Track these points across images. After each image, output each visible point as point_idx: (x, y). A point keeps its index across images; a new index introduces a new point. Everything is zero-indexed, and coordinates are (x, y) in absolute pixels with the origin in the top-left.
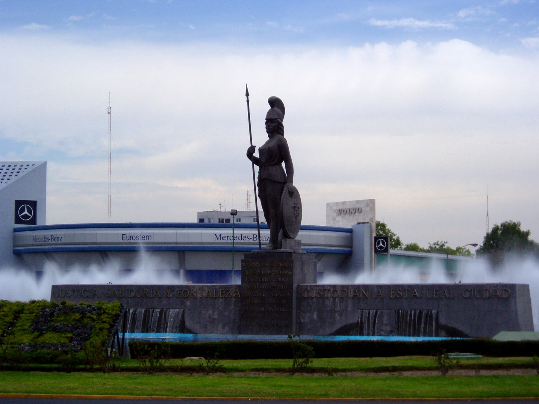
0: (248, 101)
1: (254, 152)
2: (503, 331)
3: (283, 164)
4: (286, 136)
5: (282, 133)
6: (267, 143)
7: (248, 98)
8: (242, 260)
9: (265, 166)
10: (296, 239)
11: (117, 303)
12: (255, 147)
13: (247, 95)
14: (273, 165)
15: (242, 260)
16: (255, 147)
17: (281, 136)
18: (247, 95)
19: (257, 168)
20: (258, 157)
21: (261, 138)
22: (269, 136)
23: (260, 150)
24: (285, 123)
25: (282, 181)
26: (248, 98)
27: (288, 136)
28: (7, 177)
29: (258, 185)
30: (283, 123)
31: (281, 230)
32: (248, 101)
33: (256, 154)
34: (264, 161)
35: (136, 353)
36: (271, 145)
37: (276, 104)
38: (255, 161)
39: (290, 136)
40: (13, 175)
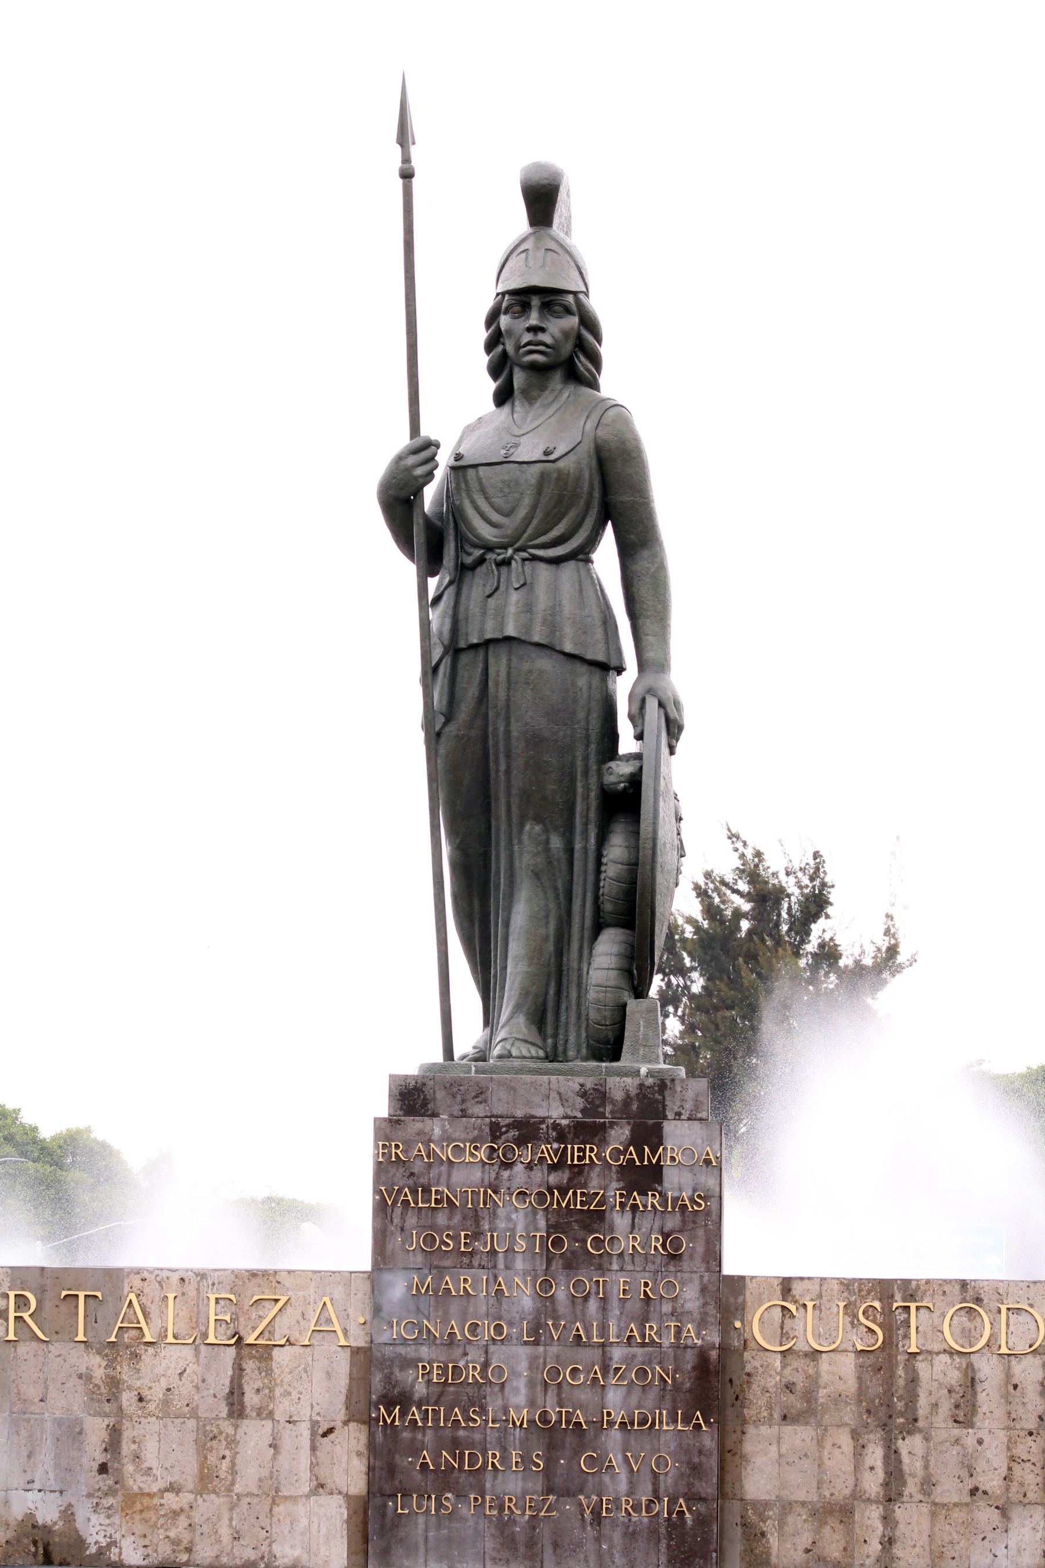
0: (407, 175)
3: (606, 558)
9: (506, 563)
14: (557, 561)
21: (462, 405)
22: (503, 397)
26: (406, 159)
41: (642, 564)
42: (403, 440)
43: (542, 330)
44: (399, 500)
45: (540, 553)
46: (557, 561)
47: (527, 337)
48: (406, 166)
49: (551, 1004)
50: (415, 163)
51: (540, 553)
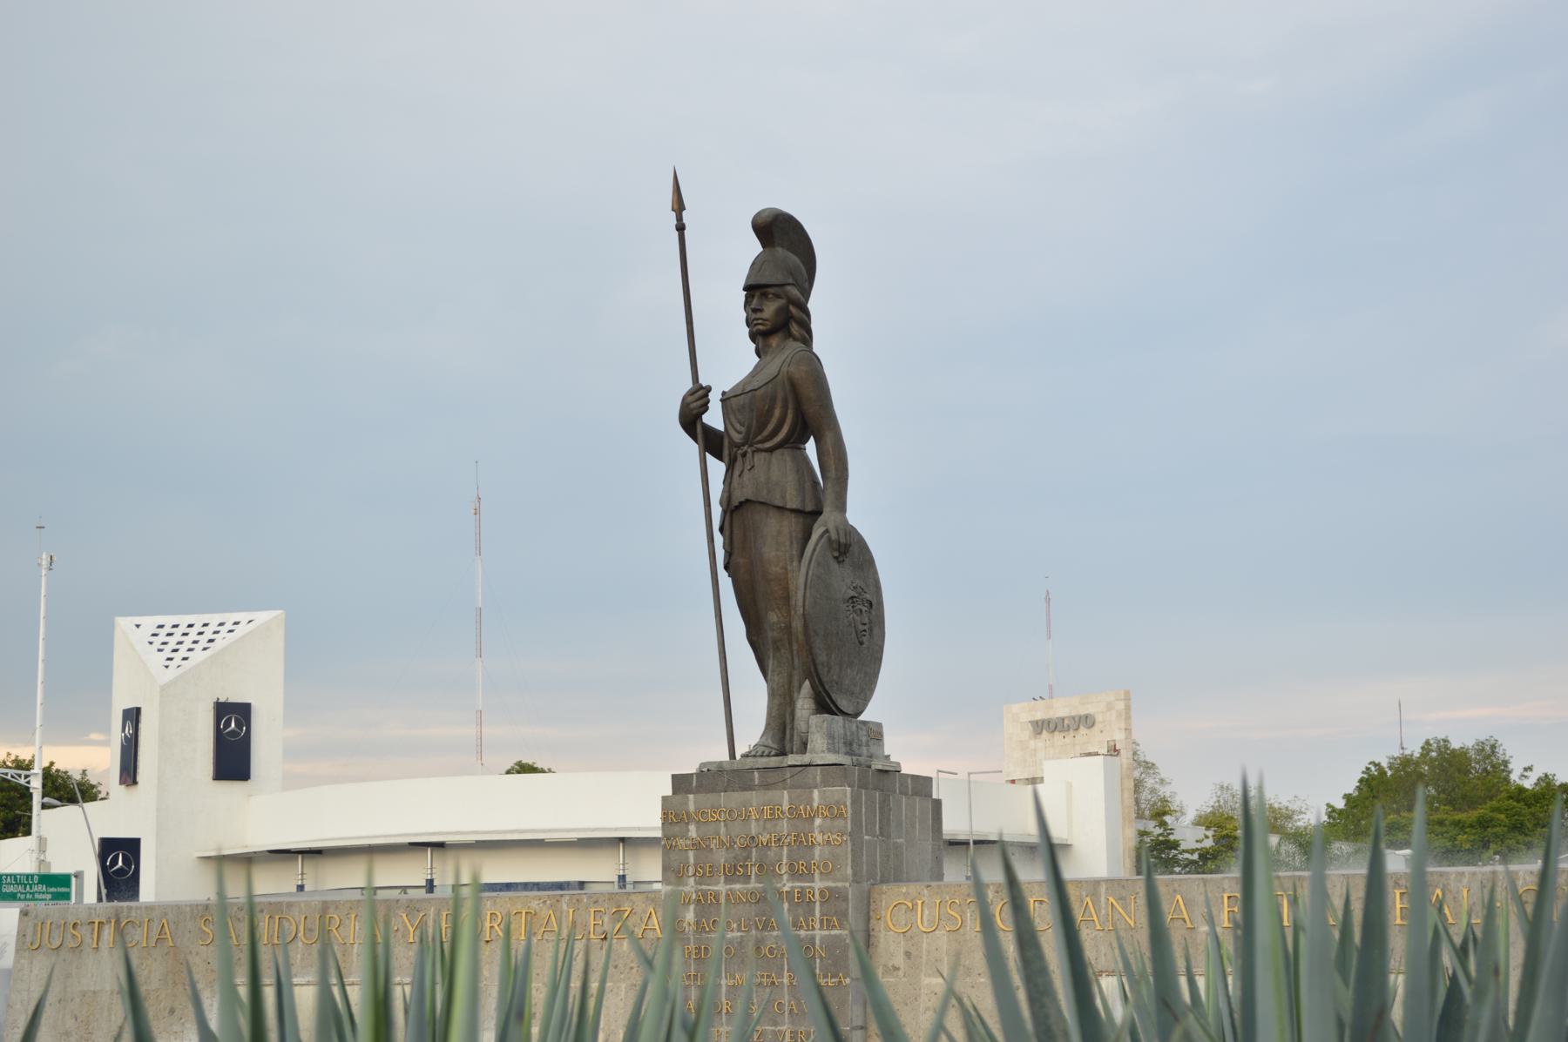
0: (681, 228)
2: (772, 694)
3: (811, 447)
4: (818, 347)
5: (807, 338)
6: (753, 374)
7: (679, 218)
8: (664, 799)
9: (744, 455)
11: (899, 960)
12: (709, 389)
13: (679, 206)
14: (771, 450)
15: (664, 799)
16: (709, 389)
17: (794, 347)
18: (679, 206)
19: (717, 468)
20: (721, 428)
21: (732, 360)
22: (758, 353)
23: (726, 399)
25: (809, 508)
26: (679, 218)
28: (183, 653)
29: (721, 530)
32: (681, 228)
33: (714, 418)
34: (737, 438)
37: (780, 233)
38: (711, 443)
40: (198, 647)
41: (829, 438)
42: (689, 385)
43: (761, 310)
44: (691, 419)
50: (685, 221)
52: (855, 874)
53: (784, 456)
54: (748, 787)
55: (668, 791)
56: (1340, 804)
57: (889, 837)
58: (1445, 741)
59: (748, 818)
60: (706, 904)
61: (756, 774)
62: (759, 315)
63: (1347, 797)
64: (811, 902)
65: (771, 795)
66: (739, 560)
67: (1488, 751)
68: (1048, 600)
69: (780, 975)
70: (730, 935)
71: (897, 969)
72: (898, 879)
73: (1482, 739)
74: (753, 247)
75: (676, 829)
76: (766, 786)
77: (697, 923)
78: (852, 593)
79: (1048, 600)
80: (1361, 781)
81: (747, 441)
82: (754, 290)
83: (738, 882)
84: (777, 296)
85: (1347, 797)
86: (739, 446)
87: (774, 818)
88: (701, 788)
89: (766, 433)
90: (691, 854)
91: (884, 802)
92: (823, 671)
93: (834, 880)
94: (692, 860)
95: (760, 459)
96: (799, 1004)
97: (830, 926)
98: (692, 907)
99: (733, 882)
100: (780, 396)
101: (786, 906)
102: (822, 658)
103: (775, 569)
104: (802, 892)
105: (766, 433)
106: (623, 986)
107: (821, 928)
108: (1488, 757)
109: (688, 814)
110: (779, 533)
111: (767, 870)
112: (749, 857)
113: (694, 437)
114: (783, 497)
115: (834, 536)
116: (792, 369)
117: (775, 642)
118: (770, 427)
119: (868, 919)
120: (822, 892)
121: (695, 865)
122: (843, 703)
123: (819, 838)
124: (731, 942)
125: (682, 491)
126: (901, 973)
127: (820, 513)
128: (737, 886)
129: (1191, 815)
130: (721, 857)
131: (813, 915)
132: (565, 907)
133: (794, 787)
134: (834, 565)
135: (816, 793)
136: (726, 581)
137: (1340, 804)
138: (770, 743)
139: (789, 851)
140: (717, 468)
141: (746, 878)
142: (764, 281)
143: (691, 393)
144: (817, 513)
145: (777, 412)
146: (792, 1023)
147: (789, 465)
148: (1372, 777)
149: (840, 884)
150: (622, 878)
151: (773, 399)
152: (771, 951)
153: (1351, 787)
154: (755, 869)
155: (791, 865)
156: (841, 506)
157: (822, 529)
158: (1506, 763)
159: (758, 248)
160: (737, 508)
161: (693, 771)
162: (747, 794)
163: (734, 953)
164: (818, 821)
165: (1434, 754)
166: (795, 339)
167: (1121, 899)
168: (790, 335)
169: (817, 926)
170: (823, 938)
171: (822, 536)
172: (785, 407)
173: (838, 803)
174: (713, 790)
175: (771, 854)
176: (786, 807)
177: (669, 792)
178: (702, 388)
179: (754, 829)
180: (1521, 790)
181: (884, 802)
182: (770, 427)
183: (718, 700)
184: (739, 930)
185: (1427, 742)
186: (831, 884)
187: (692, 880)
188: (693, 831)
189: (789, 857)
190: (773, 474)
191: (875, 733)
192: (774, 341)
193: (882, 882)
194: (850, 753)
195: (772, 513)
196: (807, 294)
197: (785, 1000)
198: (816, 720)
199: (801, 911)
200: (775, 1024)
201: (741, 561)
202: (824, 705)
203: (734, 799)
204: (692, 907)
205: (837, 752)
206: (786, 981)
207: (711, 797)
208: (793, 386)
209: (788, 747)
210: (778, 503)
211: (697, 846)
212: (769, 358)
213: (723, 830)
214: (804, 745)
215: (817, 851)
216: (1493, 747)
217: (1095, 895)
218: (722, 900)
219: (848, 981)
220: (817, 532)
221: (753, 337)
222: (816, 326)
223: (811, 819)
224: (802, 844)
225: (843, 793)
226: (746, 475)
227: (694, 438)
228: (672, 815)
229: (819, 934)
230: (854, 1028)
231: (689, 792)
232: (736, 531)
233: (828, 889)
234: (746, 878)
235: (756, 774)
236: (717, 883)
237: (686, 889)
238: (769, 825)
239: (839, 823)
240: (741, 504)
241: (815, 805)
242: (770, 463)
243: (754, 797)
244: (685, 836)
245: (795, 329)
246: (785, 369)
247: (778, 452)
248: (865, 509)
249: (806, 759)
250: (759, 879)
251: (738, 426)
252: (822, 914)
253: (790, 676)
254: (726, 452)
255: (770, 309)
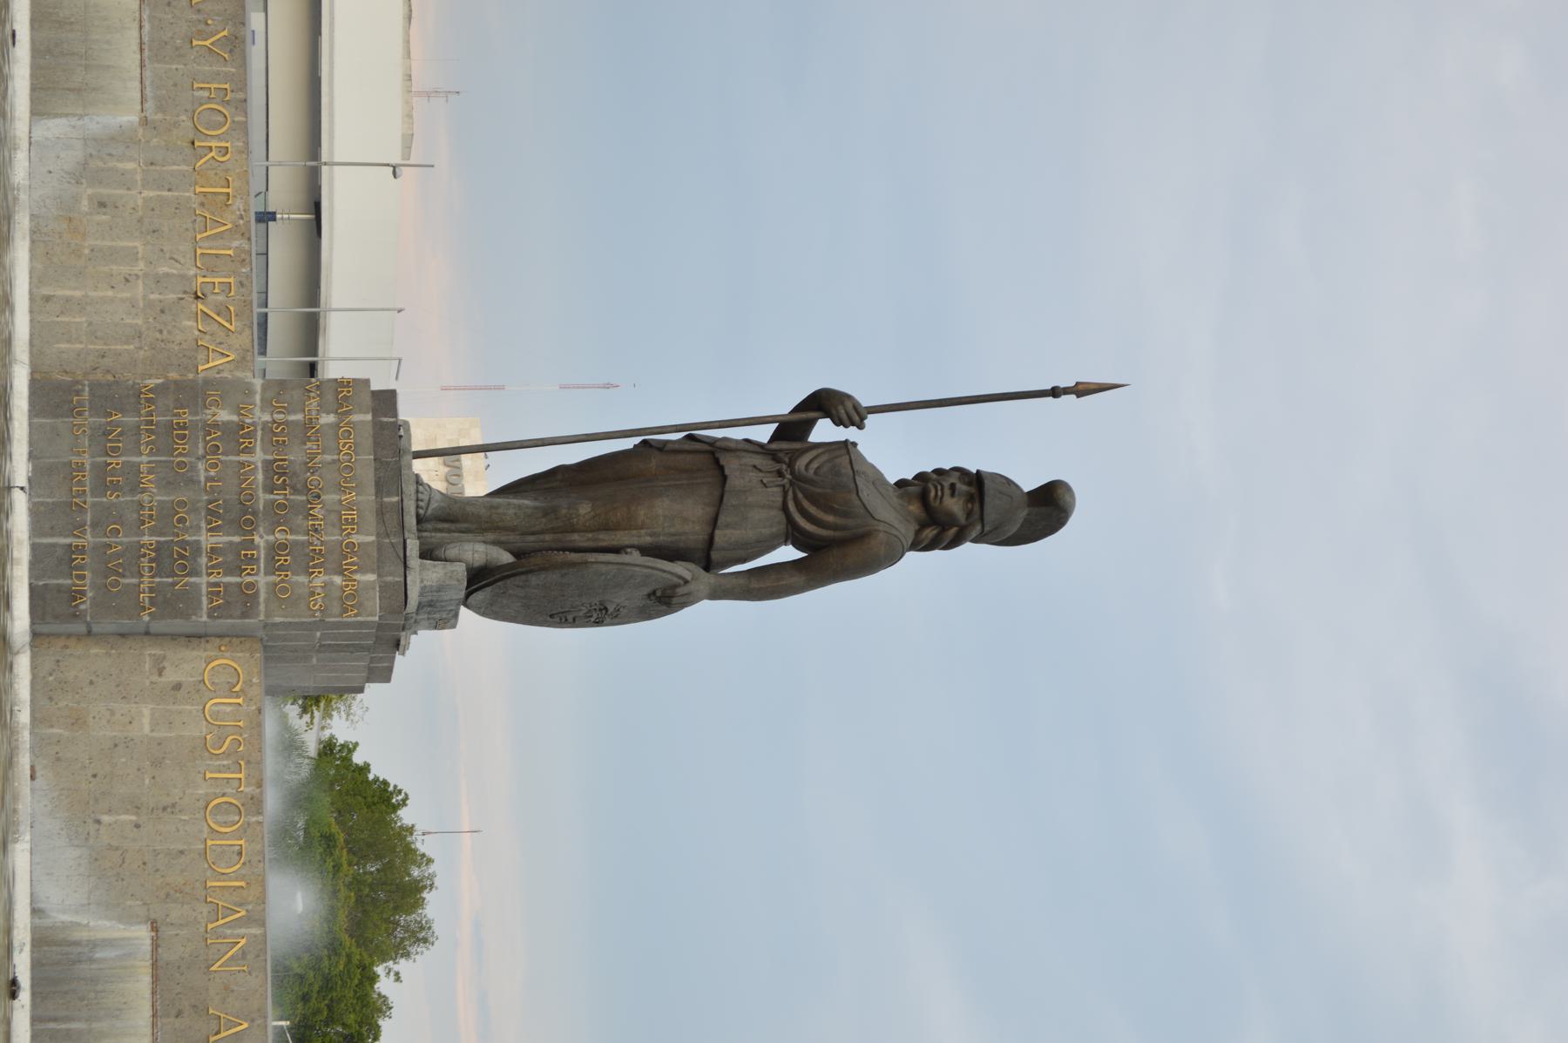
0: (1055, 392)
1: (838, 422)
3: (787, 553)
5: (918, 545)
6: (877, 478)
7: (1067, 391)
8: (367, 382)
9: (780, 474)
10: (463, 610)
11: (171, 676)
12: (861, 427)
13: (1081, 390)
14: (785, 508)
15: (367, 382)
16: (861, 427)
17: (907, 531)
18: (1081, 390)
19: (763, 434)
21: (893, 451)
22: (901, 484)
23: (847, 446)
24: (972, 554)
25: (715, 556)
26: (1067, 391)
27: (919, 572)
30: (968, 548)
31: (507, 558)
32: (1055, 392)
33: (824, 431)
34: (801, 464)
35: (299, 417)
36: (867, 494)
37: (1046, 509)
38: (792, 429)
39: (922, 584)
41: (798, 579)
42: (865, 401)
43: (953, 495)
44: (823, 403)
45: (790, 494)
46: (785, 508)
47: (946, 485)
48: (892, 517)
49: (458, 526)
50: (1064, 398)
51: (790, 494)
52: (275, 625)
53: (772, 520)
54: (380, 488)
55: (376, 386)
56: (358, 758)
57: (319, 651)
58: (432, 886)
59: (341, 490)
60: (238, 435)
61: (395, 499)
62: (947, 492)
63: (366, 768)
64: (240, 571)
65: (371, 519)
66: (654, 462)
67: (420, 935)
68: (607, 386)
69: (152, 532)
70: (201, 466)
71: (160, 675)
72: (267, 659)
73: (435, 927)
74: (1029, 482)
75: (330, 397)
76: (381, 512)
77: (216, 425)
78: (611, 609)
79: (607, 386)
80: (385, 783)
81: (797, 479)
82: (976, 483)
83: (266, 478)
84: (969, 514)
85: (366, 768)
86: (791, 465)
87: (341, 524)
88: (379, 427)
89: (806, 504)
90: (299, 417)
91: (362, 648)
92: (518, 580)
93: (267, 601)
94: (292, 418)
95: (775, 494)
96: (118, 555)
97: (213, 595)
98: (235, 418)
99: (266, 471)
100: (850, 522)
101: (237, 539)
102: (534, 579)
103: (642, 513)
104: (252, 560)
105: (806, 504)
106: (140, 322)
107: (210, 585)
108: (414, 933)
109: (348, 413)
110: (685, 520)
111: (278, 516)
112: (295, 491)
113: (798, 408)
114: (727, 526)
115: (680, 591)
116: (881, 535)
117: (555, 510)
118: (812, 510)
119: (220, 636)
120: (251, 585)
121: (287, 423)
122: (478, 597)
123: (319, 581)
124: (193, 468)
125: (741, 397)
126: (155, 678)
127: (707, 568)
128: (260, 477)
129: (340, 729)
130: (295, 456)
131: (225, 574)
132: (236, 244)
133: (380, 547)
134: (646, 590)
135: (371, 577)
136: (628, 444)
137: (358, 758)
138: (434, 505)
139: (303, 543)
140: (763, 434)
141: (270, 488)
142: (987, 499)
143: (856, 406)
144: (708, 566)
145: (830, 518)
146: (95, 548)
147: (766, 531)
148: (389, 799)
149: (262, 607)
150: (272, 216)
151: (846, 515)
152: (181, 520)
153: (377, 771)
154: (280, 499)
155: (283, 546)
156: (716, 594)
157: (688, 576)
158: (407, 955)
159: (1027, 488)
160: (717, 461)
161: (402, 416)
162: (372, 490)
163: (176, 477)
164: (338, 580)
165: (416, 873)
166: (918, 533)
167: (244, 953)
168: (923, 526)
169: (212, 579)
170: (197, 586)
171: (680, 577)
172: (835, 528)
173: (360, 605)
174: (376, 444)
175: (299, 520)
176: (355, 539)
177: (375, 386)
178: (862, 419)
179: (330, 498)
180: (373, 978)
181: (362, 648)
182: (812, 510)
183: (480, 423)
184: (208, 479)
185: (430, 861)
186: (262, 597)
187: (267, 417)
188: (328, 419)
189: (296, 543)
190: (757, 498)
191: (446, 620)
192: (915, 508)
193: (265, 647)
194: (420, 606)
195: (710, 510)
196: (975, 541)
197: (122, 538)
198: (460, 570)
199: (230, 558)
200: (94, 525)
201: (654, 463)
202: (479, 578)
203: (367, 475)
204: (235, 418)
205: (421, 595)
206: (146, 539)
207: (368, 443)
208: (861, 537)
209: (429, 526)
210: (722, 519)
211: (309, 425)
212: (895, 501)
213: (328, 458)
214: (427, 554)
215: (302, 579)
216: (425, 940)
217: (248, 921)
218: (243, 458)
219: (146, 618)
220: (680, 568)
221: (921, 477)
222: (937, 555)
223: (341, 572)
224: (308, 560)
225: (372, 612)
226: (754, 476)
227: (797, 409)
228: (346, 392)
229: (203, 581)
230: (88, 625)
231: (375, 413)
232: (689, 457)
233: (256, 594)
234: (270, 488)
235: (395, 499)
236: (265, 451)
237: (257, 412)
238: (333, 517)
239: (336, 610)
240: (722, 468)
241: (357, 577)
242: (771, 507)
243: (368, 498)
244: (322, 408)
245: (930, 533)
246: (881, 527)
247: (781, 517)
248: (709, 621)
249: (414, 561)
250: (271, 504)
251: (815, 465)
252: (227, 585)
253: (513, 530)
254: (784, 445)
255: (954, 505)
